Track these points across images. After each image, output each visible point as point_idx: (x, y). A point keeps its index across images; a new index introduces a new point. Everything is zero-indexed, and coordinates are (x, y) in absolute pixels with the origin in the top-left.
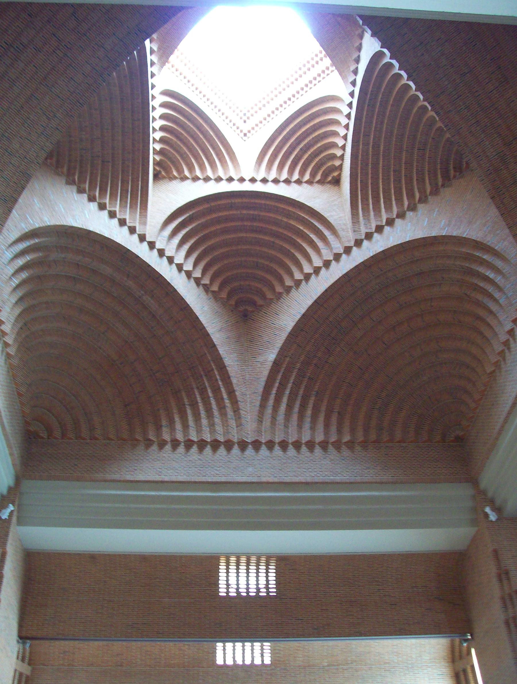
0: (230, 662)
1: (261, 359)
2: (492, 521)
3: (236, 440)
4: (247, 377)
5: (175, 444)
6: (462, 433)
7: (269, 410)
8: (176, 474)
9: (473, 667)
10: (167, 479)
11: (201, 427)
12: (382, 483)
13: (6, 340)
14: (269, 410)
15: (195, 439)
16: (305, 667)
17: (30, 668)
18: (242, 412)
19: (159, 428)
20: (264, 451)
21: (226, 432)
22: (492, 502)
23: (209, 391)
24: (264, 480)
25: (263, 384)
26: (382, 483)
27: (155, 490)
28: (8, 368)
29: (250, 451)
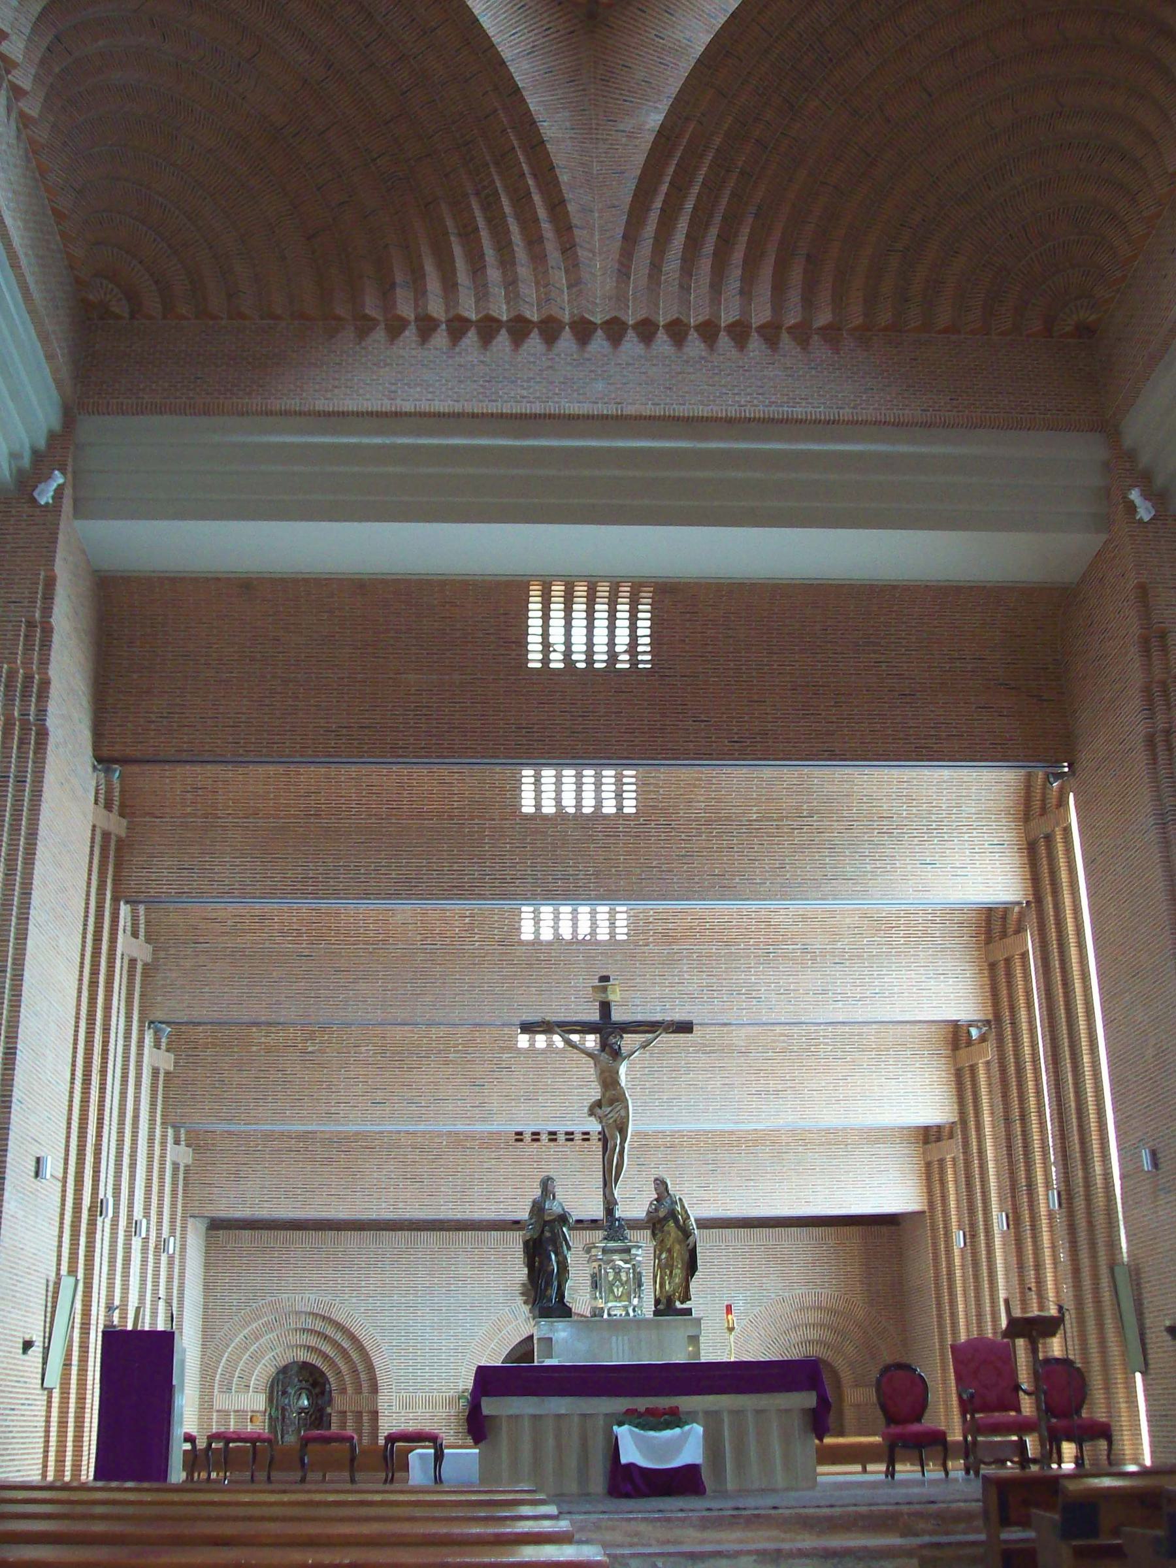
0: (549, 808)
1: (628, 124)
2: (1141, 521)
3: (567, 318)
4: (596, 167)
5: (427, 327)
6: (1093, 317)
7: (645, 249)
8: (430, 396)
9: (1067, 830)
10: (408, 407)
11: (485, 286)
12: (898, 424)
13: (14, 80)
14: (645, 249)
15: (473, 317)
16: (709, 822)
17: (150, 948)
18: (580, 252)
19: (387, 291)
20: (631, 344)
21: (545, 300)
22: (1145, 480)
23: (505, 201)
24: (630, 410)
25: (632, 185)
26: (898, 424)
27: (379, 432)
28: (26, 150)
29: (599, 343)
